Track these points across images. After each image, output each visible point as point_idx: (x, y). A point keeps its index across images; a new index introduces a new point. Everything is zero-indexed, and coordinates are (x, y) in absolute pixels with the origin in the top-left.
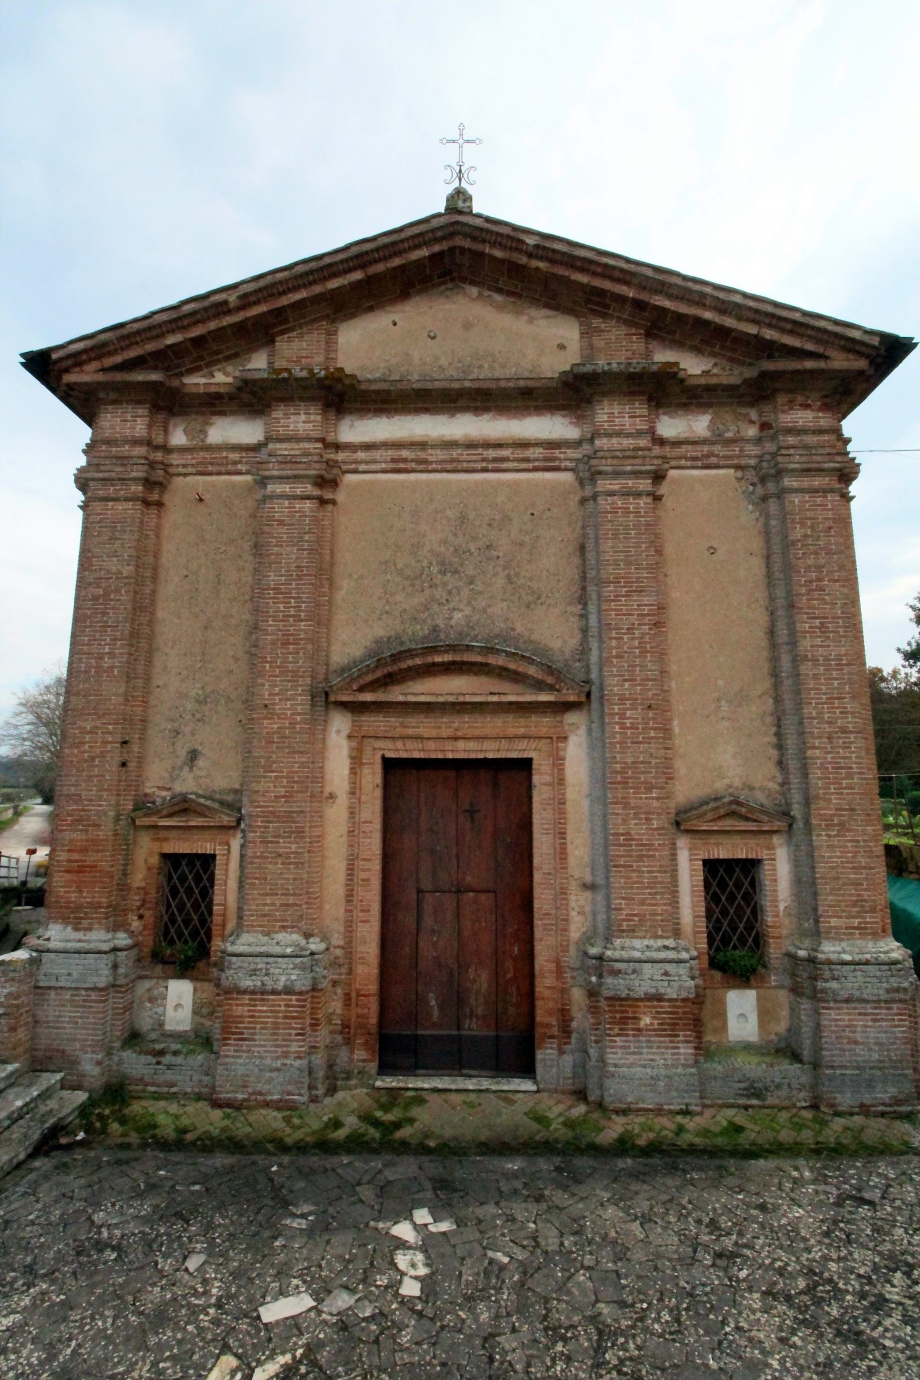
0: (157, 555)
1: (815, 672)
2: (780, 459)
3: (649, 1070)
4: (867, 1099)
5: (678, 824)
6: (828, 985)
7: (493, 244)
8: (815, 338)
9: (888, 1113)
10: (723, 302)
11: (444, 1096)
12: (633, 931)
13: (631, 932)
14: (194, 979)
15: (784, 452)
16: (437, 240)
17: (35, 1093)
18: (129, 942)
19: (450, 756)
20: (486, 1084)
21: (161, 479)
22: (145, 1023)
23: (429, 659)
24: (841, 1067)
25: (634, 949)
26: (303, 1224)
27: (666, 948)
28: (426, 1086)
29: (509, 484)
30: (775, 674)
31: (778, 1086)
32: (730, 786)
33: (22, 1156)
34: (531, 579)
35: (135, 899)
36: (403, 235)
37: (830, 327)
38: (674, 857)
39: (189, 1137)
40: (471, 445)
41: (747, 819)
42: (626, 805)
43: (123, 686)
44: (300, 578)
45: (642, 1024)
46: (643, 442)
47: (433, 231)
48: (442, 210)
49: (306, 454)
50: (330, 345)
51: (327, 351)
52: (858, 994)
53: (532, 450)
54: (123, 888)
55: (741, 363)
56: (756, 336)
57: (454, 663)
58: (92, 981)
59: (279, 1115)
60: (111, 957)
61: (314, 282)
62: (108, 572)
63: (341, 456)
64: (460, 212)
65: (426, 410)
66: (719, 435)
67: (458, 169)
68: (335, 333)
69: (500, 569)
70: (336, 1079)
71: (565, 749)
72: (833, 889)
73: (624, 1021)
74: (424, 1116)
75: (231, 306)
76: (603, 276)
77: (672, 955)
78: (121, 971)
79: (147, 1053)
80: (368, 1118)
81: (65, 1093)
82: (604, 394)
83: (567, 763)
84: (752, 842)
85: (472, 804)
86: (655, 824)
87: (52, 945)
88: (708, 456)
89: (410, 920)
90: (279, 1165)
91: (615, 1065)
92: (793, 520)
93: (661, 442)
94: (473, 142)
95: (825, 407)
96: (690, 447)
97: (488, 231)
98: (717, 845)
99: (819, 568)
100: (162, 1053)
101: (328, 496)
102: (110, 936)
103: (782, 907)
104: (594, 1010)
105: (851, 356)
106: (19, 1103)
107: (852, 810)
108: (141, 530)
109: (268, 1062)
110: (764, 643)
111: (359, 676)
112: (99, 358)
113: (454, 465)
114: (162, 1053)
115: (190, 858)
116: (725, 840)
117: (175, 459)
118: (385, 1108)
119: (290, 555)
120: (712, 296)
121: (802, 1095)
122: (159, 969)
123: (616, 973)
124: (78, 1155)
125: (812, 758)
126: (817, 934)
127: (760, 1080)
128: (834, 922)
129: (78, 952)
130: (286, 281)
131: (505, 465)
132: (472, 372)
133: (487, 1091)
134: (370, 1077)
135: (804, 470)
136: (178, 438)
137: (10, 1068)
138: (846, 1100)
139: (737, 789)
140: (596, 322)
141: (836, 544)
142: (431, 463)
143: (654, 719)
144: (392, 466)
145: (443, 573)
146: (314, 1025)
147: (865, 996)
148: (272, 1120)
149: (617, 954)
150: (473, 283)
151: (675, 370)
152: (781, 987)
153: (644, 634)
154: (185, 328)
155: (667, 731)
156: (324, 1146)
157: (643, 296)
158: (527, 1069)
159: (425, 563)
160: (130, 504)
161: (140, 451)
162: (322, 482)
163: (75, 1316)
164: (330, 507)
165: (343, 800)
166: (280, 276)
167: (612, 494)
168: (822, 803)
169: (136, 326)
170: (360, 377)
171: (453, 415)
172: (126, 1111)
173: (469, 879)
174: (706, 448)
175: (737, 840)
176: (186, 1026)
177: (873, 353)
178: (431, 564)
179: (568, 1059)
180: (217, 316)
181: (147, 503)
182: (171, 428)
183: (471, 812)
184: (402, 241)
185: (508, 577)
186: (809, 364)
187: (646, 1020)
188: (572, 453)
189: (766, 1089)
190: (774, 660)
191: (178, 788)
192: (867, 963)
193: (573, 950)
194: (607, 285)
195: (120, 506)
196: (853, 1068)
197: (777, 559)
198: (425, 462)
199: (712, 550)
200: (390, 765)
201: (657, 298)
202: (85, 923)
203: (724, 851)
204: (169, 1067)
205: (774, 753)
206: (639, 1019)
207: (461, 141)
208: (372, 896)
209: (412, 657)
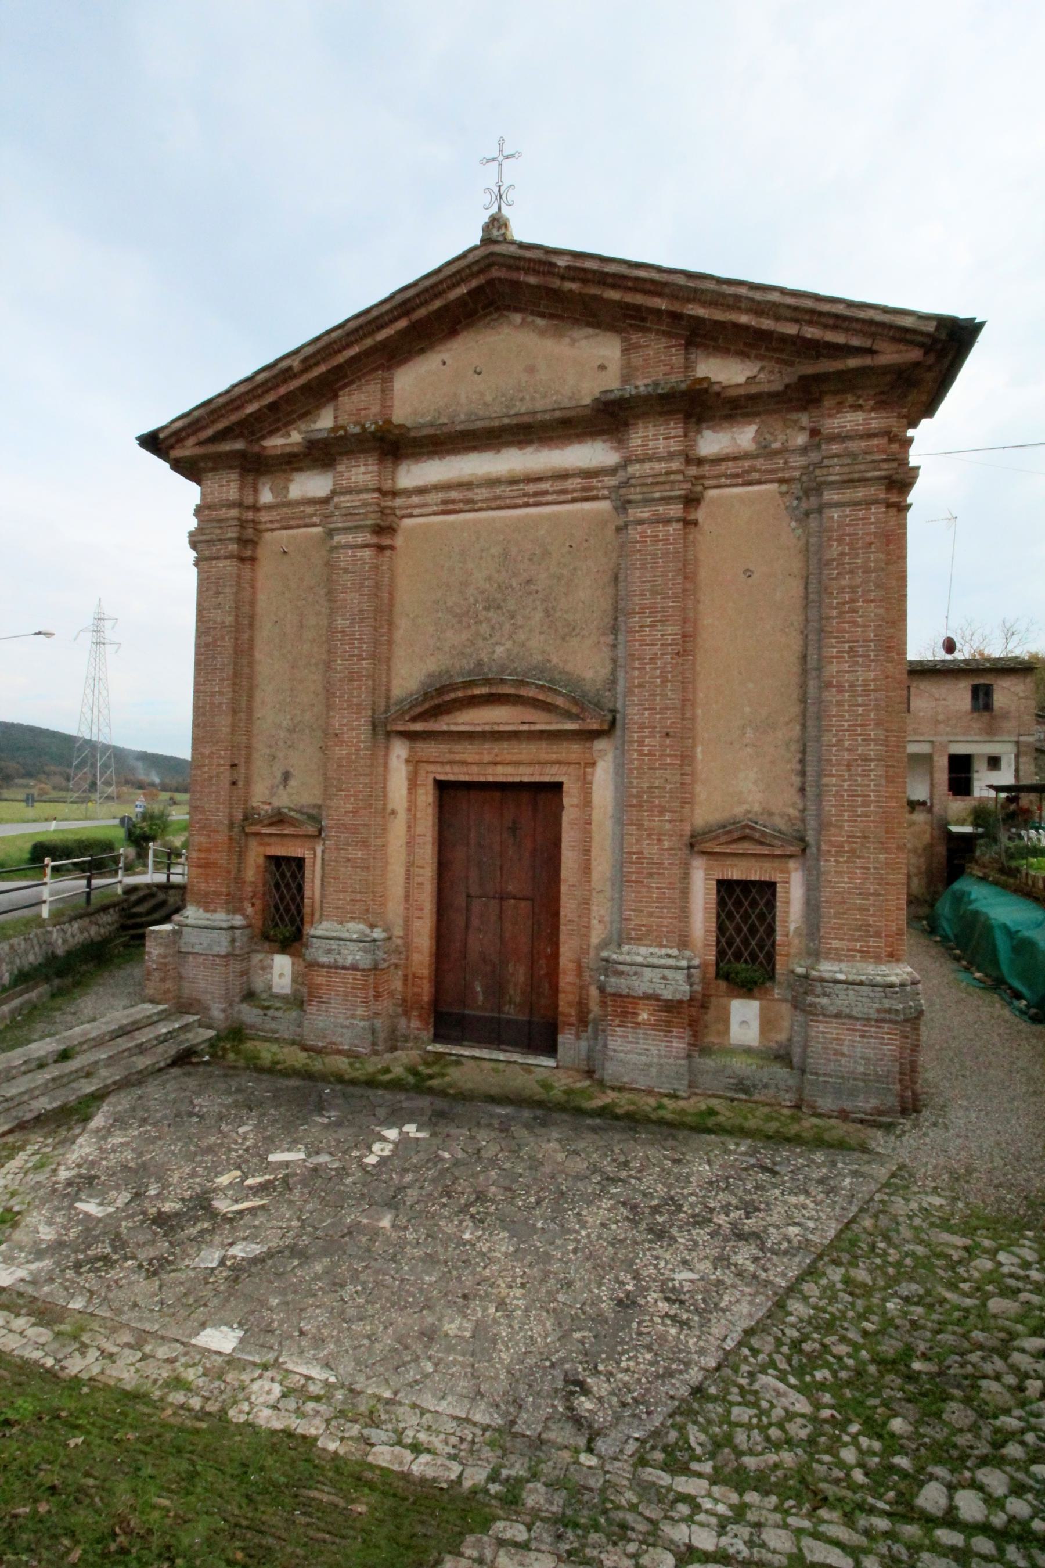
0: (253, 603)
1: (839, 698)
2: (818, 472)
3: (643, 1058)
4: (848, 1106)
5: (692, 845)
6: (817, 1000)
7: (528, 271)
8: (861, 331)
9: (867, 1121)
10: (759, 303)
11: (478, 1062)
12: (640, 939)
13: (638, 940)
14: (292, 955)
15: (826, 462)
16: (474, 275)
17: (177, 1026)
18: (244, 922)
19: (491, 779)
20: (516, 1057)
21: (251, 537)
22: (258, 985)
23: (469, 692)
24: (825, 1075)
25: (638, 954)
26: (326, 1120)
27: (669, 956)
28: (466, 1053)
29: (549, 517)
30: (803, 700)
31: (766, 1086)
32: (749, 812)
33: (162, 1064)
34: (567, 612)
35: (249, 890)
36: (441, 276)
37: (879, 317)
38: (686, 877)
39: (279, 1067)
40: (513, 481)
41: (761, 843)
42: (640, 826)
43: (230, 718)
44: (362, 620)
45: (640, 1019)
46: (675, 465)
47: (469, 266)
48: (478, 243)
49: (365, 504)
50: (386, 391)
51: (383, 400)
52: (847, 1011)
53: (570, 481)
54: (239, 881)
55: (791, 364)
56: (798, 336)
57: (492, 695)
58: (216, 950)
59: (346, 1060)
60: (230, 932)
61: (365, 336)
62: (215, 622)
63: (398, 502)
64: (496, 242)
65: (474, 449)
66: (765, 447)
67: (496, 190)
68: (391, 380)
69: (538, 603)
70: (397, 1041)
71: (593, 774)
72: (837, 913)
73: (624, 1014)
74: (454, 1074)
75: (296, 370)
76: (635, 290)
77: (671, 962)
78: (237, 944)
79: (258, 1007)
80: (413, 1071)
81: (201, 1030)
82: (638, 417)
83: (595, 787)
84: (767, 865)
85: (514, 822)
86: (666, 845)
87: (190, 921)
88: (748, 472)
89: (460, 920)
90: (332, 1090)
91: (615, 1051)
92: (830, 539)
93: (700, 462)
94: (512, 156)
95: (881, 405)
96: (730, 464)
97: (520, 258)
98: (732, 866)
99: (853, 589)
100: (268, 1008)
101: (386, 541)
102: (230, 917)
103: (792, 927)
104: (603, 1004)
105: (902, 347)
106: (164, 1031)
107: (865, 837)
108: (238, 584)
109: (340, 1020)
110: (796, 669)
111: (411, 708)
112: (194, 433)
113: (498, 502)
114: (268, 1008)
115: (288, 859)
116: (743, 863)
117: (264, 517)
118: (427, 1064)
119: (353, 599)
120: (748, 298)
121: (787, 1096)
122: (267, 945)
123: (620, 974)
124: (201, 1069)
125: (827, 786)
126: (816, 955)
127: (748, 1078)
128: (836, 944)
129: (206, 928)
130: (340, 339)
131: (544, 499)
132: (514, 405)
133: (515, 1062)
134: (423, 1043)
135: (845, 482)
136: (266, 497)
137: (161, 1007)
138: (826, 1103)
139: (756, 814)
140: (635, 337)
141: (876, 561)
142: (476, 502)
143: (671, 746)
144: (441, 507)
145: (487, 609)
146: (377, 997)
147: (854, 1013)
148: (341, 1063)
149: (621, 958)
150: (517, 310)
151: (705, 385)
152: (785, 1000)
153: (666, 663)
154: (259, 397)
155: (686, 758)
156: (371, 1083)
157: (676, 307)
158: (550, 1049)
159: (472, 600)
160: (228, 562)
161: (234, 513)
162: (379, 530)
163: (160, 1143)
164: (388, 553)
165: (402, 817)
166: (334, 335)
167: (641, 522)
168: (833, 830)
169: (221, 400)
170: (409, 424)
171: (499, 451)
172: (242, 1047)
173: (510, 888)
174: (747, 464)
175: (753, 862)
176: (287, 991)
177: (928, 341)
178: (476, 601)
179: (583, 1045)
180: (285, 381)
181: (242, 560)
182: (260, 485)
183: (514, 830)
184: (441, 282)
185: (546, 611)
186: (853, 363)
187: (644, 1016)
188: (610, 481)
189: (755, 1086)
190: (803, 686)
191: (277, 803)
192: (861, 983)
193: (592, 953)
194: (639, 299)
195: (221, 564)
196: (837, 1077)
197: (813, 579)
198: (471, 501)
199: (748, 573)
200: (442, 786)
201: (690, 306)
202: (212, 907)
203: (736, 873)
204: (273, 1018)
205: (797, 780)
206: (636, 1014)
207: (501, 158)
208: (426, 898)
209: (455, 690)
